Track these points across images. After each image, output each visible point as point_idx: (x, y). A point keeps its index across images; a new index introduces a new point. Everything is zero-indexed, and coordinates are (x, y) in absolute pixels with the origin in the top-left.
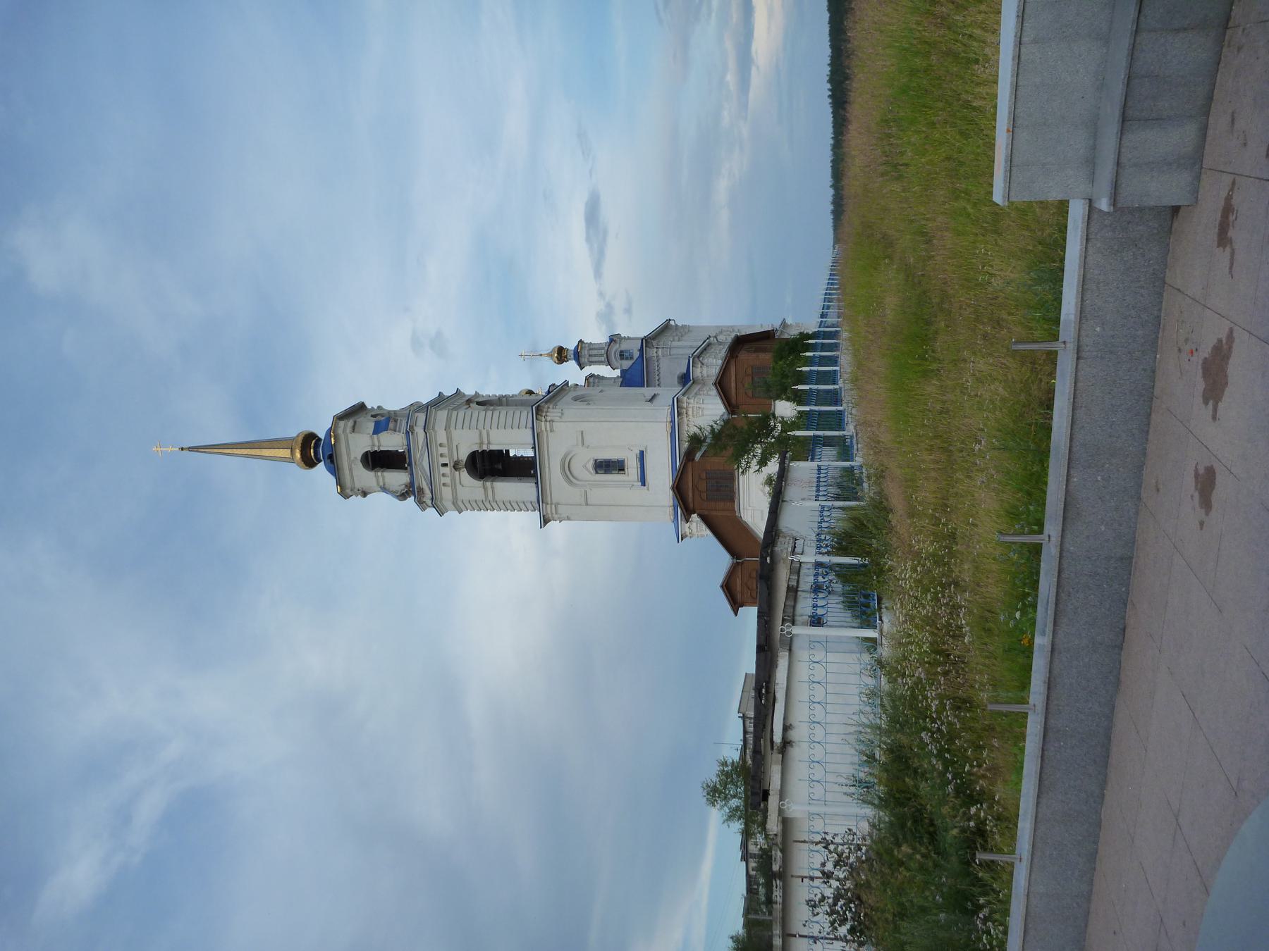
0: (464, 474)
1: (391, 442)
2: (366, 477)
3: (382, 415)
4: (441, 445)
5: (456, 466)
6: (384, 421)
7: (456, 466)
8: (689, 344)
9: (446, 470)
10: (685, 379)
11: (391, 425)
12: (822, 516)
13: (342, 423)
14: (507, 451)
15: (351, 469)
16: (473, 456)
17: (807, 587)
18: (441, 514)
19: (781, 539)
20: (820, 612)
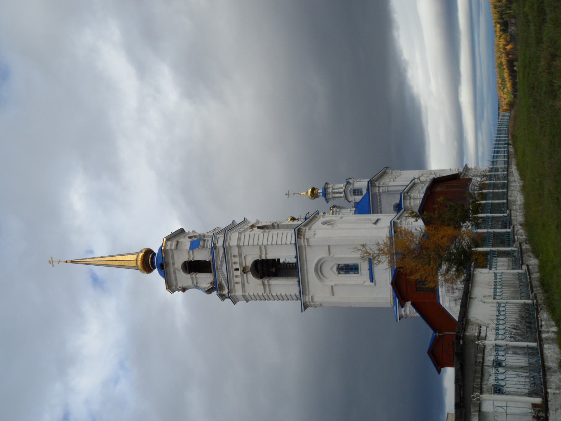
0: (250, 275)
1: (201, 255)
2: (184, 278)
3: (195, 237)
4: (234, 256)
5: (244, 271)
6: (197, 241)
7: (244, 271)
8: (401, 183)
9: (238, 273)
10: (398, 208)
11: (201, 244)
12: (499, 311)
13: (169, 243)
14: (279, 260)
15: (175, 274)
16: (256, 264)
17: (490, 364)
18: (235, 303)
19: (470, 326)
20: (500, 358)
